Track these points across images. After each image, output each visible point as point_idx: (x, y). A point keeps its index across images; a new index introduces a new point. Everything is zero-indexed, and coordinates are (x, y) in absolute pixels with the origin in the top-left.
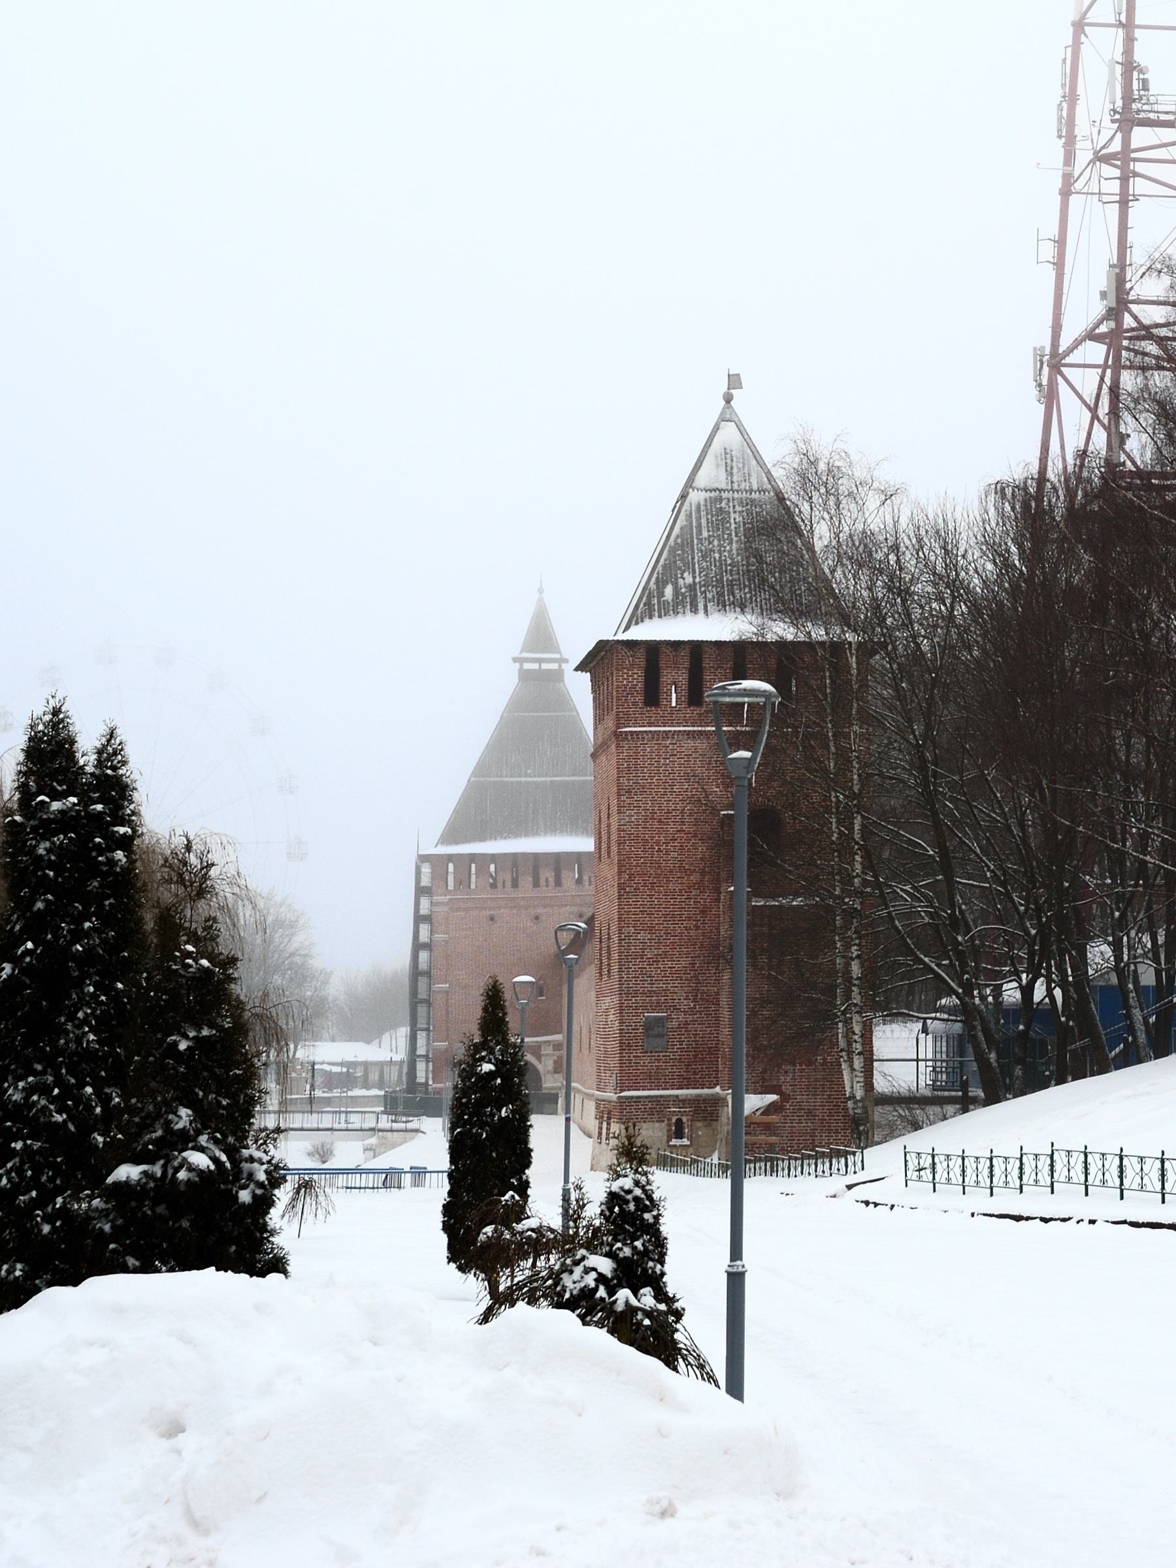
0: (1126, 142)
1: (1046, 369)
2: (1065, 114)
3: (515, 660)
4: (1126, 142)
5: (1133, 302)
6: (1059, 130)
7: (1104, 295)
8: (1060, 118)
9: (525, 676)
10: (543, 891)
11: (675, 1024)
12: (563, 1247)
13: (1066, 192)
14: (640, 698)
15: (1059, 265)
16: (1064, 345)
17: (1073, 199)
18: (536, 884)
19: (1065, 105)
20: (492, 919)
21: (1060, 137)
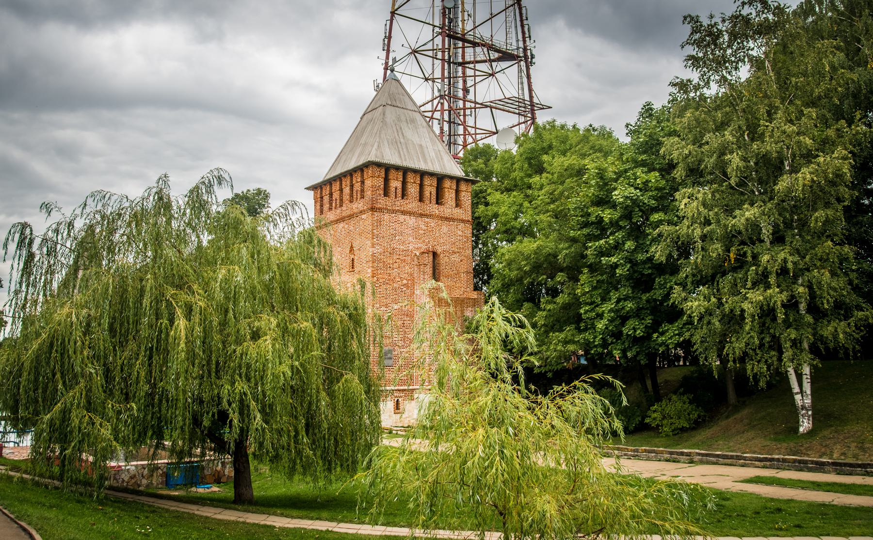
14: (382, 192)
19: (386, 40)
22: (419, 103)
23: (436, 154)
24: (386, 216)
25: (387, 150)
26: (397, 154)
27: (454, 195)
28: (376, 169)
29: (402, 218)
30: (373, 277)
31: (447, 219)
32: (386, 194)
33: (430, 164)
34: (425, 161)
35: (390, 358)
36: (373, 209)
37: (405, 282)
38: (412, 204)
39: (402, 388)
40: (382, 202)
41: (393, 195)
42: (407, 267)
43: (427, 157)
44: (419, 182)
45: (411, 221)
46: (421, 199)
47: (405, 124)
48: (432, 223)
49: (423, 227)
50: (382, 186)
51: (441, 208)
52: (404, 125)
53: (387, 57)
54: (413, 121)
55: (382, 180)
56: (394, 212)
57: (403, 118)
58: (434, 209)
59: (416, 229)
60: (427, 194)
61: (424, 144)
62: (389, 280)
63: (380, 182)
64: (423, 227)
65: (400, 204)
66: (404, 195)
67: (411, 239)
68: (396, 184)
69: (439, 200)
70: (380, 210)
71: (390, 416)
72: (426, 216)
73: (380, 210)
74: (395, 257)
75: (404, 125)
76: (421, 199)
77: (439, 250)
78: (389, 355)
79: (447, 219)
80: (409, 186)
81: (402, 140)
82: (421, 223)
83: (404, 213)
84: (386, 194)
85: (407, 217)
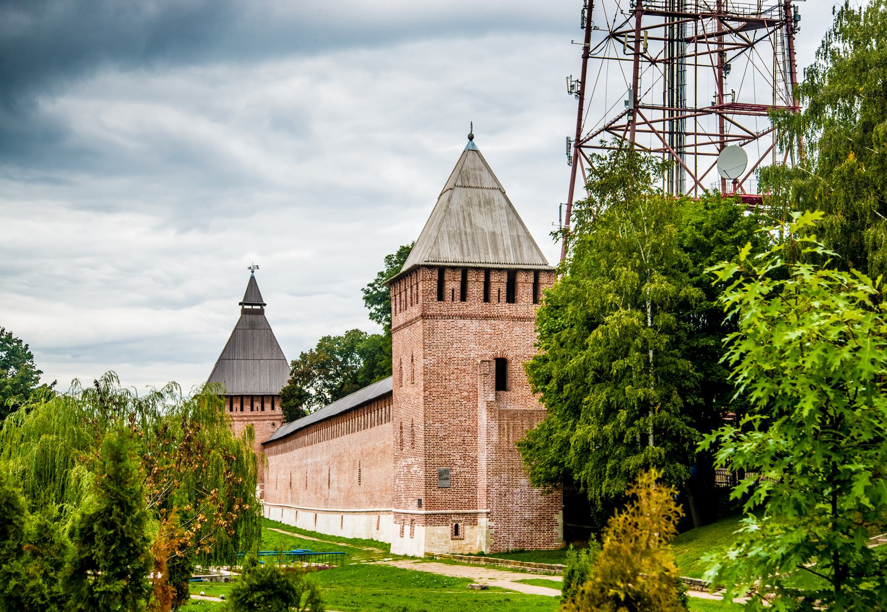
0: (638, 23)
1: (573, 149)
2: (586, 15)
3: (240, 304)
4: (638, 23)
5: (641, 107)
6: (583, 24)
7: (626, 103)
8: (583, 18)
9: (244, 312)
10: (255, 413)
11: (454, 473)
12: (115, 534)
13: (586, 57)
14: (435, 296)
15: (581, 95)
16: (583, 136)
17: (589, 60)
18: (252, 410)
19: (586, 11)
20: (274, 425)
21: (582, 28)
22: (662, 118)
23: (513, 242)
24: (441, 323)
25: (447, 245)
26: (458, 249)
27: (530, 290)
28: (428, 274)
29: (461, 323)
30: (425, 391)
31: (519, 319)
32: (441, 297)
33: (502, 256)
34: (496, 251)
35: (447, 479)
36: (424, 316)
37: (465, 394)
38: (475, 305)
39: (461, 511)
40: (436, 307)
41: (494, 299)
42: (468, 378)
43: (500, 247)
44: (483, 280)
45: (473, 325)
46: (487, 299)
47: (477, 208)
48: (501, 325)
49: (489, 331)
50: (435, 290)
51: (513, 306)
52: (474, 211)
53: (588, 39)
54: (489, 202)
55: (436, 283)
56: (449, 317)
57: (475, 201)
58: (505, 308)
59: (479, 334)
60: (494, 292)
61: (498, 231)
62: (445, 393)
63: (434, 286)
64: (489, 331)
65: (458, 306)
66: (463, 298)
67: (472, 345)
68: (452, 285)
69: (511, 297)
70: (433, 317)
71: (446, 542)
72: (493, 318)
73: (433, 317)
74: (452, 367)
75: (474, 211)
76: (487, 299)
77: (510, 355)
78: (445, 476)
79: (519, 319)
80: (470, 285)
81: (469, 230)
82: (486, 326)
83: (463, 317)
84: (441, 297)
85: (467, 322)
